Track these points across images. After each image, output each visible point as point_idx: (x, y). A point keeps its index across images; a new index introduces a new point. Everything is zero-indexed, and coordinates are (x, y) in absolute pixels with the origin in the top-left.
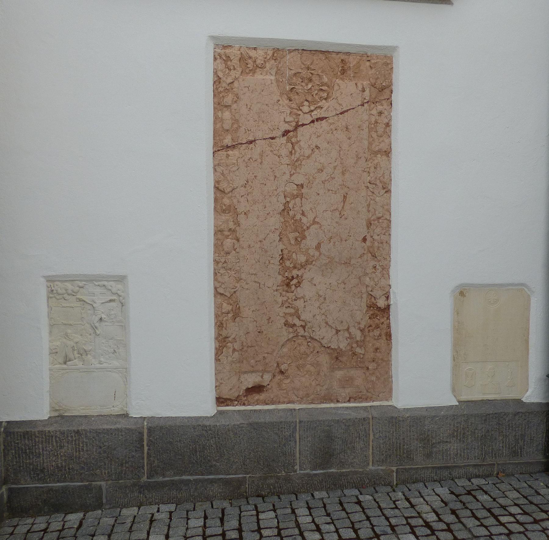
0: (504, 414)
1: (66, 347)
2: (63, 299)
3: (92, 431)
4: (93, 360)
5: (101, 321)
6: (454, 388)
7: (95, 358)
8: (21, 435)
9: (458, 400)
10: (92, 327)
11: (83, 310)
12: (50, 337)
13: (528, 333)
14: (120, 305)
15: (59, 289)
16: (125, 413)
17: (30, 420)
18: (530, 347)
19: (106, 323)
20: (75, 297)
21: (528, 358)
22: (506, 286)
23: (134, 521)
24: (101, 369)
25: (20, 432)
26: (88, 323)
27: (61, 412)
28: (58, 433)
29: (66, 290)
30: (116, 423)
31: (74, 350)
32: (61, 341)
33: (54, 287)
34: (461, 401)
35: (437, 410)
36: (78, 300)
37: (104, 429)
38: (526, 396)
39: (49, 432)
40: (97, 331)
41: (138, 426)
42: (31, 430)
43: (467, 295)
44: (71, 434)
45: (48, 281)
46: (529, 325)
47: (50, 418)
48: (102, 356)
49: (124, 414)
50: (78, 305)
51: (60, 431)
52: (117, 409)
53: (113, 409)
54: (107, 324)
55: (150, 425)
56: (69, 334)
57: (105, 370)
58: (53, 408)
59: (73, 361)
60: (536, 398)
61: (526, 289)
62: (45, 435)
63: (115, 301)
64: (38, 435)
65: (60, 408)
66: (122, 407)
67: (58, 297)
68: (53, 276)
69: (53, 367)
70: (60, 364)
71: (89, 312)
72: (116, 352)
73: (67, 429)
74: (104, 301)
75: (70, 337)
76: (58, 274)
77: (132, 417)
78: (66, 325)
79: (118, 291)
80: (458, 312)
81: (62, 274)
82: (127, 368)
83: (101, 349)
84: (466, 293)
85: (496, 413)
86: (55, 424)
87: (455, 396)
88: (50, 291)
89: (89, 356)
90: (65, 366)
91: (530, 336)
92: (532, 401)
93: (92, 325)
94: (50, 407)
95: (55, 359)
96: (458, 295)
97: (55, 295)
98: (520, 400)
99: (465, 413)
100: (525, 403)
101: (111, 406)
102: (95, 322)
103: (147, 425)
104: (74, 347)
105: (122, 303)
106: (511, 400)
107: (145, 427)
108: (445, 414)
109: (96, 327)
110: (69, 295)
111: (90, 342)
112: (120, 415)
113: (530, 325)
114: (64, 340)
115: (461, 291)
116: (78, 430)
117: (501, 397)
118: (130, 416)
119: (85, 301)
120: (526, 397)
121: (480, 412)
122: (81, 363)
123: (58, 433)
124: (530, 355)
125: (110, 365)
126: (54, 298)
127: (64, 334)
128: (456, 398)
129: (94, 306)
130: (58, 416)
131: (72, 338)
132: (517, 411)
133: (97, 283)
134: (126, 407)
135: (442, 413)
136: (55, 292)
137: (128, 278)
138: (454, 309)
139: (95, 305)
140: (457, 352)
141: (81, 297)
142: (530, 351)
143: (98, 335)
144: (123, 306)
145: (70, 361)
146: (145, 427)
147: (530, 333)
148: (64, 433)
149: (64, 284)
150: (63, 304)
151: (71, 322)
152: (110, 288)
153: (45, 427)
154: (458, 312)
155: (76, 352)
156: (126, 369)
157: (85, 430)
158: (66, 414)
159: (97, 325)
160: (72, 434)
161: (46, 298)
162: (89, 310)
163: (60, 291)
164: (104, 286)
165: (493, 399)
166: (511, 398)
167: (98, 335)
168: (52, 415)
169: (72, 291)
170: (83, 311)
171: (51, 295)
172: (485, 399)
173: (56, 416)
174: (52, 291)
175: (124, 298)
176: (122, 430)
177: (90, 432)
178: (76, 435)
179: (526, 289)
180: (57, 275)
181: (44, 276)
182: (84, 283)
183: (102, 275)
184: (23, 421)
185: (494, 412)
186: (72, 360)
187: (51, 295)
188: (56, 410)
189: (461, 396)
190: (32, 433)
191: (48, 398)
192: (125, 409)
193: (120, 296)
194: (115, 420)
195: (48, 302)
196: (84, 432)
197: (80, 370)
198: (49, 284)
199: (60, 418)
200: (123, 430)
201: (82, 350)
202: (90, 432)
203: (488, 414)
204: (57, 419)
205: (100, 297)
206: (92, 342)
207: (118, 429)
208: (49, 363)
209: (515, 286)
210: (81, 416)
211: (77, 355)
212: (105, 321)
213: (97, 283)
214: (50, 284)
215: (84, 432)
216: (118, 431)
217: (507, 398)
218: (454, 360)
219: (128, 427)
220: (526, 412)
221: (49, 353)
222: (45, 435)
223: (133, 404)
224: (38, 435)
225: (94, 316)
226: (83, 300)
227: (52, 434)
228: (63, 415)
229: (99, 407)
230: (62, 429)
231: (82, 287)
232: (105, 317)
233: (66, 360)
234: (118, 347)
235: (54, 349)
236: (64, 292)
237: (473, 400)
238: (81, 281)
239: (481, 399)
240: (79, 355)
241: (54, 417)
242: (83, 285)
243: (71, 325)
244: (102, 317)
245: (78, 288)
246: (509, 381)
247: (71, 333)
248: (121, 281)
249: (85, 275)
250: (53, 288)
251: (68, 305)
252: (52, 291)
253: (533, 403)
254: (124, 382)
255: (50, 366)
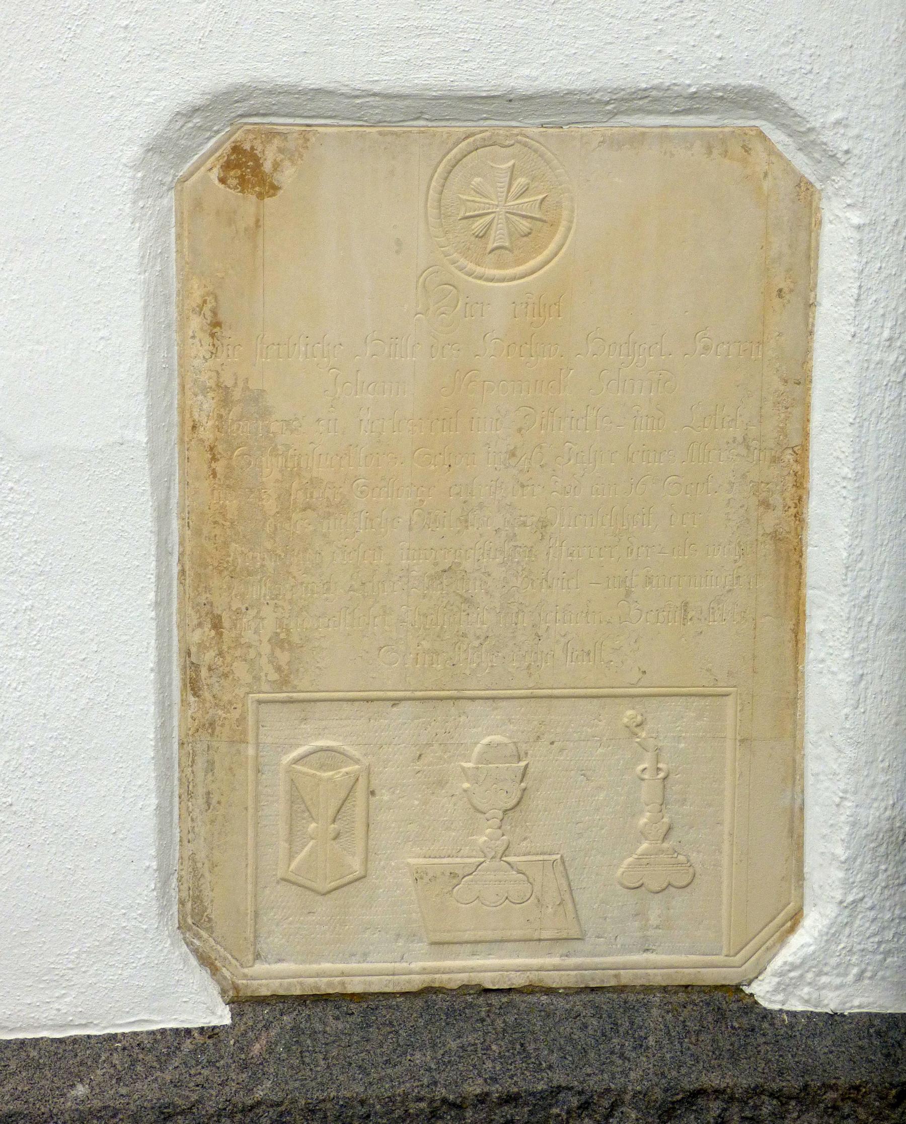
0: (575, 1102)
6: (197, 899)
9: (236, 988)
13: (800, 481)
18: (810, 594)
21: (797, 678)
22: (614, 114)
23: (440, 205)
34: (261, 1001)
35: (39, 1067)
38: (777, 963)
43: (287, 176)
46: (806, 420)
60: (860, 977)
61: (777, 137)
80: (215, 313)
84: (276, 166)
85: (510, 1099)
87: (206, 961)
91: (814, 508)
92: (831, 1003)
96: (214, 175)
98: (737, 989)
99: (259, 1094)
100: (767, 1015)
106: (665, 989)
108: (97, 1104)
113: (816, 418)
115: (236, 149)
117: (577, 968)
120: (781, 974)
121: (385, 1090)
124: (814, 651)
128: (214, 971)
132: (689, 1084)
135: (81, 1090)
138: (184, 293)
140: (217, 625)
142: (815, 624)
147: (816, 481)
154: (215, 313)
165: (519, 980)
166: (658, 978)
172: (455, 980)
179: (777, 137)
185: (496, 1090)
189: (257, 957)
203: (444, 1101)
209: (687, 112)
217: (627, 977)
218: (193, 685)
220: (757, 1091)
237: (356, 986)
239: (416, 982)
246: (645, 846)
253: (833, 1019)
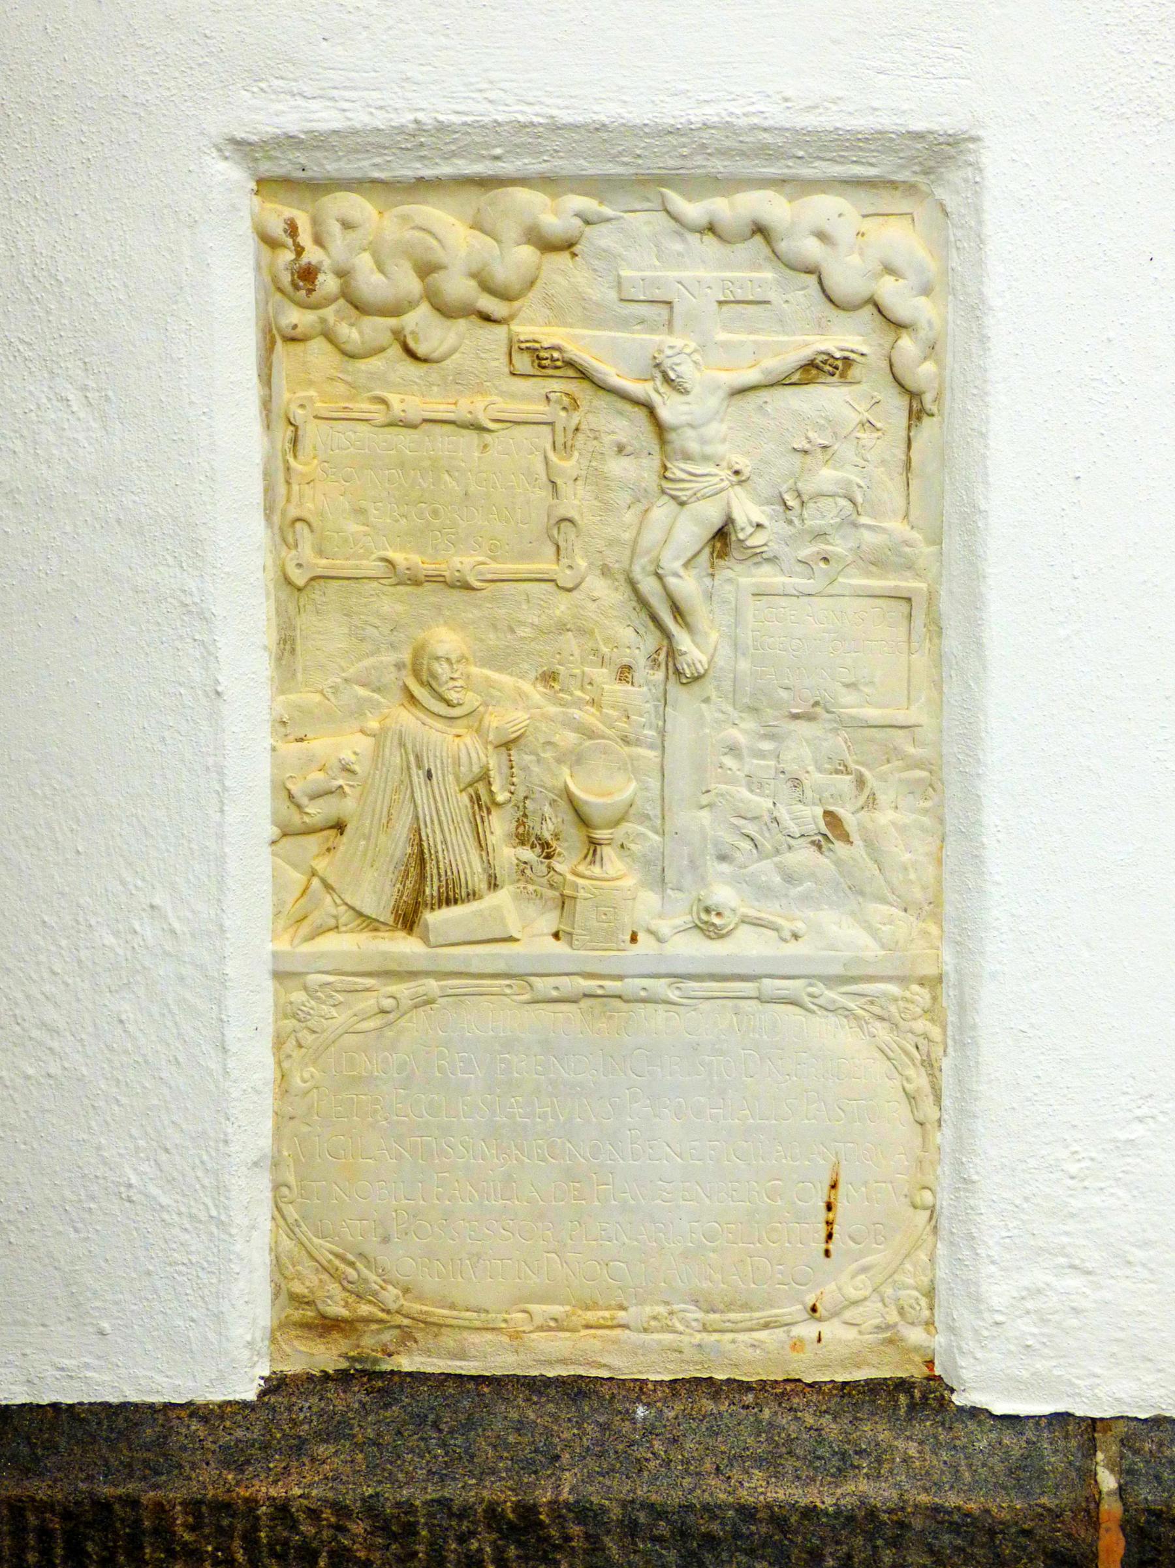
1: (418, 777)
2: (396, 350)
3: (642, 1517)
4: (649, 899)
5: (723, 554)
7: (661, 882)
8: (44, 1533)
10: (642, 602)
11: (566, 449)
12: (282, 691)
14: (897, 405)
15: (365, 261)
16: (916, 1372)
17: (114, 1399)
19: (767, 568)
20: (500, 331)
24: (713, 977)
25: (43, 1507)
26: (605, 571)
27: (369, 1342)
28: (358, 1528)
29: (426, 269)
30: (844, 1466)
31: (482, 805)
32: (373, 725)
33: (318, 241)
36: (523, 363)
37: (747, 1513)
39: (282, 1510)
40: (684, 641)
41: (1044, 1500)
42: (131, 1487)
44: (462, 1539)
45: (265, 185)
47: (275, 1385)
48: (725, 867)
49: (903, 1385)
50: (539, 409)
51: (371, 1508)
52: (851, 1334)
53: (808, 1330)
54: (766, 576)
55: (1146, 1494)
56: (442, 669)
57: (748, 988)
58: (296, 1299)
59: (474, 906)
62: (250, 1541)
63: (854, 372)
64: (187, 1537)
65: (365, 1309)
66: (893, 1317)
67: (351, 333)
68: (319, 141)
69: (307, 948)
70: (370, 923)
71: (617, 467)
72: (846, 838)
73: (432, 1493)
74: (752, 376)
75: (453, 696)
76: (361, 118)
77: (975, 1413)
78: (417, 583)
79: (888, 280)
81: (398, 120)
82: (940, 979)
83: (710, 805)
86: (322, 1450)
88: (286, 279)
89: (613, 863)
90: (406, 946)
93: (649, 586)
94: (276, 1294)
95: (327, 886)
97: (329, 313)
101: (795, 1310)
102: (672, 563)
103: (1121, 1488)
104: (485, 777)
105: (913, 395)
107: (1111, 1508)
109: (412, 698)
110: (446, 311)
111: (626, 741)
112: (873, 1387)
114: (407, 719)
116: (527, 1511)
118: (958, 1400)
119: (583, 374)
122: (548, 921)
123: (358, 1528)
125: (792, 948)
126: (318, 345)
127: (399, 666)
129: (664, 414)
130: (344, 1378)
131: (471, 700)
133: (693, 210)
134: (929, 1324)
136: (328, 283)
137: (985, 159)
139: (670, 409)
141: (549, 335)
143: (697, 678)
144: (917, 414)
145: (448, 899)
146: (1111, 1508)
148: (410, 1530)
149: (405, 218)
150: (393, 398)
151: (463, 562)
152: (812, 249)
153: (240, 1469)
155: (499, 826)
156: (934, 982)
157: (583, 1512)
158: (406, 1363)
159: (687, 586)
160: (474, 1545)
161: (248, 341)
162: (621, 449)
163: (377, 277)
164: (760, 230)
167: (697, 678)
168: (292, 1367)
169: (474, 275)
170: (568, 465)
171: (295, 317)
173: (326, 1377)
174: (308, 275)
175: (932, 349)
176: (901, 1525)
177: (631, 1529)
178: (512, 1551)
180: (355, 132)
181: (238, 144)
182: (579, 202)
183: (754, 128)
184: (55, 1406)
186: (472, 896)
187: (295, 317)
188: (327, 1326)
190: (138, 1522)
191: (264, 1213)
192: (915, 1336)
193: (898, 326)
194: (832, 1429)
195: (266, 377)
196: (575, 1530)
197: (538, 982)
198: (276, 215)
199: (357, 1395)
200: (917, 1523)
201: (548, 810)
202: (631, 1529)
204: (340, 1401)
205: (722, 336)
206: (638, 743)
207: (872, 1514)
208: (277, 914)
210: (535, 1386)
211: (507, 854)
212: (758, 557)
213: (693, 210)
214: (289, 212)
215: (575, 1530)
216: (870, 1537)
219: (953, 1500)
221: (272, 831)
222: (250, 1541)
223: (995, 1302)
224: (187, 1537)
225: (662, 511)
226: (570, 364)
227: (307, 1529)
228: (386, 1367)
229: (694, 1314)
230: (390, 1494)
231: (568, 246)
232: (758, 514)
233: (419, 891)
234: (861, 782)
235: (314, 797)
236: (410, 284)
238: (549, 183)
240: (527, 854)
241: (310, 1378)
242: (578, 222)
243: (467, 587)
244: (729, 521)
245: (527, 253)
247: (462, 659)
248: (911, 189)
249: (260, 369)
250: (313, 255)
251: (441, 410)
252: (308, 275)
254: (911, 1098)
255: (283, 945)
